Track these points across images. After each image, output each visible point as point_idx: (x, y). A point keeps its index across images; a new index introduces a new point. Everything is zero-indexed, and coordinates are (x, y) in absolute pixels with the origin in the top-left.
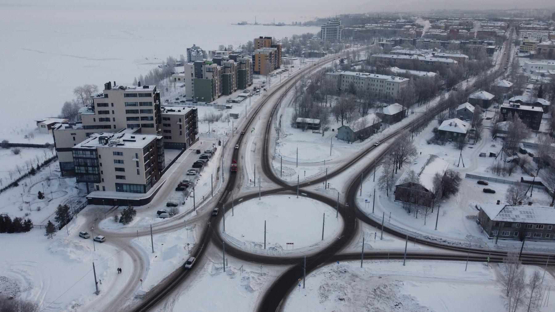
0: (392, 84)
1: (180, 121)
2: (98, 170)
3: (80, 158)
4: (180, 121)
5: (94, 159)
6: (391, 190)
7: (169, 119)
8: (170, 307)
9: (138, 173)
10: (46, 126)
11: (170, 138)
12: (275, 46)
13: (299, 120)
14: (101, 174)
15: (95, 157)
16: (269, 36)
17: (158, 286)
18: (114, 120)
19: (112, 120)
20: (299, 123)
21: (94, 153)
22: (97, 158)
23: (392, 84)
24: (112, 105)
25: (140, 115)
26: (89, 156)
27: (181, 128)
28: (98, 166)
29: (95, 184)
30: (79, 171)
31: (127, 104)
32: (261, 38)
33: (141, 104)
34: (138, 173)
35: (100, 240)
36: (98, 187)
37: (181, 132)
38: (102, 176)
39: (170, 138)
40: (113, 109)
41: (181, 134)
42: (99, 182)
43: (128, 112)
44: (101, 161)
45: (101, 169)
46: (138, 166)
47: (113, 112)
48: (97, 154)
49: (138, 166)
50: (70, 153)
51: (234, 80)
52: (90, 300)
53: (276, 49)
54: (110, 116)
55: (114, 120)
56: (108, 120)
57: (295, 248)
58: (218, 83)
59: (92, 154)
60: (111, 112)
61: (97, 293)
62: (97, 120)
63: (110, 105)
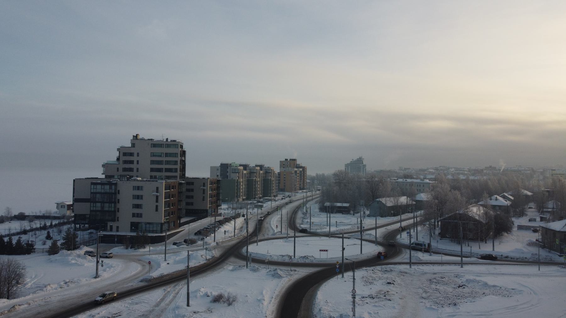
0: (422, 185)
1: (204, 186)
2: (115, 207)
3: (98, 193)
4: (204, 186)
5: (112, 193)
6: (434, 233)
7: (193, 184)
8: (181, 287)
9: (157, 210)
10: (66, 207)
11: (192, 204)
12: (301, 167)
13: (327, 204)
14: (117, 213)
15: (113, 191)
16: (294, 158)
17: (168, 275)
18: (138, 155)
19: (135, 170)
20: (326, 207)
21: (113, 187)
22: (115, 194)
23: (422, 185)
24: (138, 154)
25: (164, 166)
26: (108, 191)
27: (204, 193)
28: (115, 203)
29: (110, 224)
30: (94, 209)
31: (153, 155)
32: (286, 160)
33: (167, 155)
34: (157, 210)
35: (107, 255)
36: (111, 227)
37: (204, 197)
38: (118, 215)
39: (192, 204)
40: (138, 158)
41: (203, 200)
42: (113, 220)
43: (153, 162)
44: (119, 197)
45: (118, 206)
46: (157, 201)
47: (138, 162)
48: (116, 189)
49: (157, 201)
50: (88, 204)
51: (259, 187)
52: (86, 280)
53: (301, 169)
54: (135, 158)
55: (138, 155)
56: (132, 162)
57: (330, 256)
58: (243, 187)
59: (110, 188)
60: (135, 162)
61: (97, 276)
62: (121, 169)
63: (135, 155)
